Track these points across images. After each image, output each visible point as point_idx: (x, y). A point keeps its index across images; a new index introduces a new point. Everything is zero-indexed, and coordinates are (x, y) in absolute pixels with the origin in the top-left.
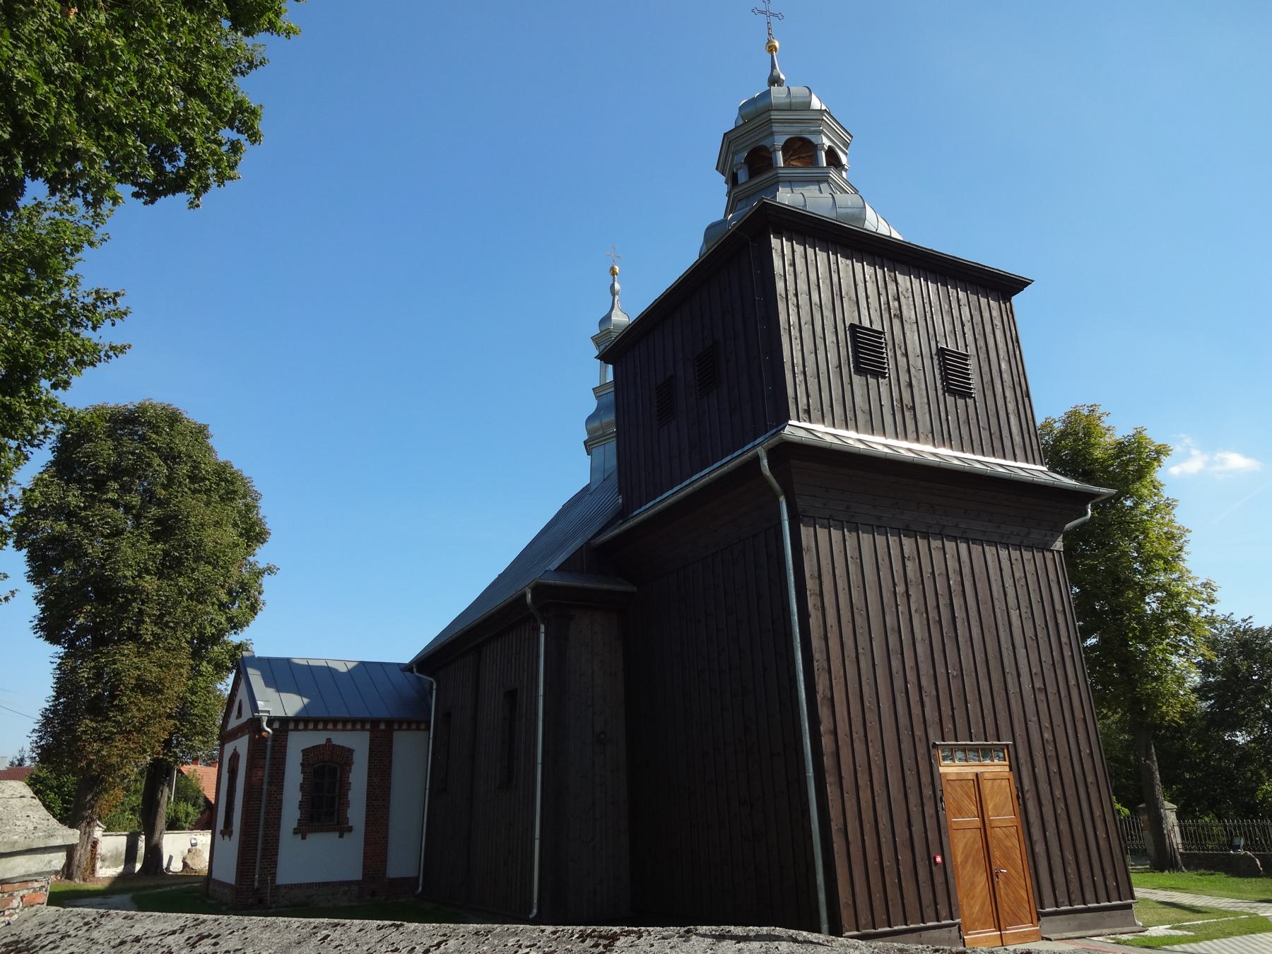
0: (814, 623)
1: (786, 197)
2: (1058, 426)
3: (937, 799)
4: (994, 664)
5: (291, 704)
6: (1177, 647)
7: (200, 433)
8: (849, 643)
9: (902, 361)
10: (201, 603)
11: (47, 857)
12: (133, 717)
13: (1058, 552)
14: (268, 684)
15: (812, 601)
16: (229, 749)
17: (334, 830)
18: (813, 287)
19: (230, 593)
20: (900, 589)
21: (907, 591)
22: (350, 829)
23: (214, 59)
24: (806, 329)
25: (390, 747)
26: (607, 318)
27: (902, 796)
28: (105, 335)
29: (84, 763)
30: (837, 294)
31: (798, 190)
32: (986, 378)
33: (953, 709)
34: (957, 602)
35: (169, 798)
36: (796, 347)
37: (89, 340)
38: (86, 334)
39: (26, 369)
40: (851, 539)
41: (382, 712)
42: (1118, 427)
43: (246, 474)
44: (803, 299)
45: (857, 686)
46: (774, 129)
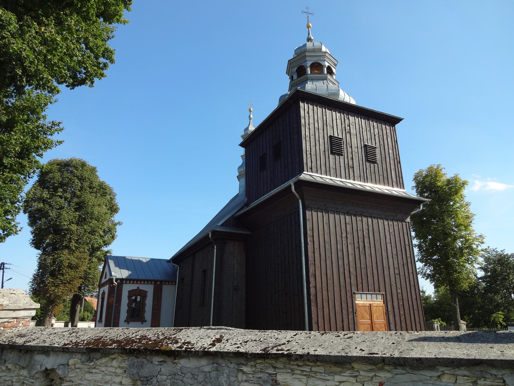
0: (310, 247)
1: (310, 87)
2: (424, 173)
3: (354, 313)
4: (379, 264)
5: (124, 274)
6: (468, 260)
9: (349, 150)
10: (93, 235)
11: (30, 311)
12: (67, 278)
13: (408, 222)
14: (116, 266)
15: (309, 239)
17: (140, 321)
18: (316, 121)
19: (104, 231)
20: (344, 235)
21: (347, 236)
22: (146, 321)
23: (95, 36)
24: (312, 138)
25: (161, 291)
26: (247, 129)
27: (340, 311)
28: (55, 137)
29: (48, 295)
30: (325, 124)
31: (315, 83)
32: (383, 156)
33: (362, 280)
34: (366, 240)
35: (81, 310)
36: (308, 144)
37: (50, 139)
38: (49, 137)
39: (27, 150)
40: (326, 216)
41: (158, 277)
43: (111, 186)
44: (312, 126)
45: (325, 270)
46: (307, 59)
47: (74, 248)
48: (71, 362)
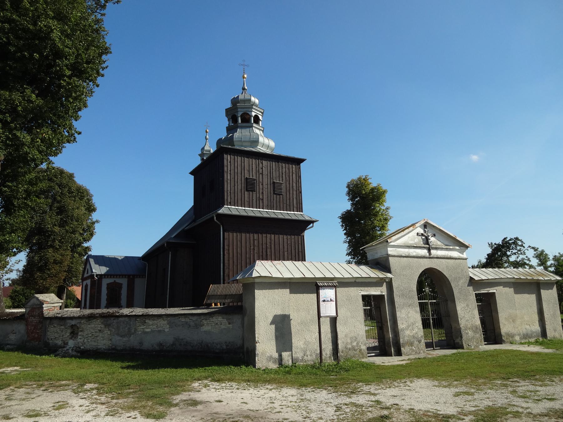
0: (226, 257)
7: (71, 176)
8: (235, 261)
16: (85, 283)
19: (83, 230)
20: (252, 248)
26: (203, 149)
34: (268, 250)
42: (373, 183)
47: (58, 247)
48: (82, 321)
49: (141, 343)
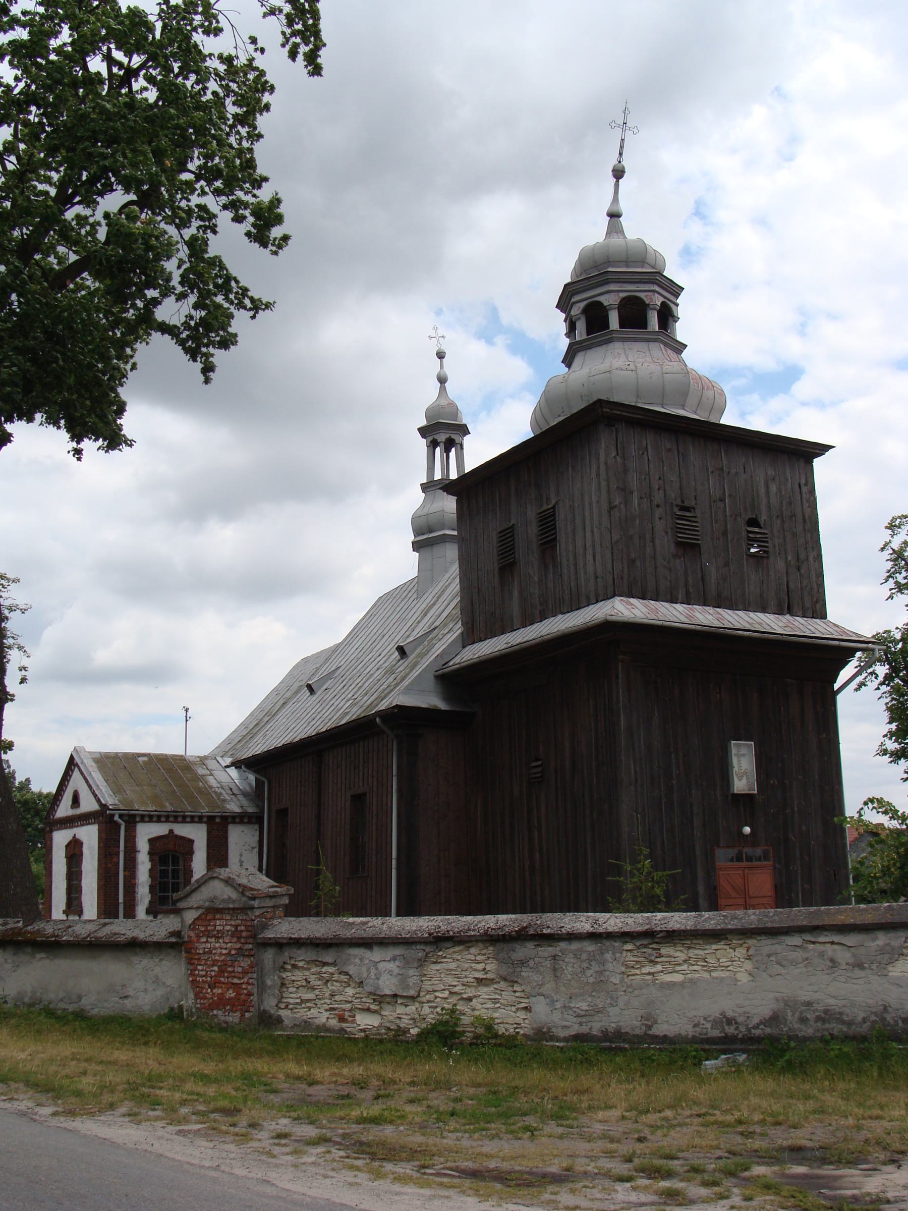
49: (649, 1020)
